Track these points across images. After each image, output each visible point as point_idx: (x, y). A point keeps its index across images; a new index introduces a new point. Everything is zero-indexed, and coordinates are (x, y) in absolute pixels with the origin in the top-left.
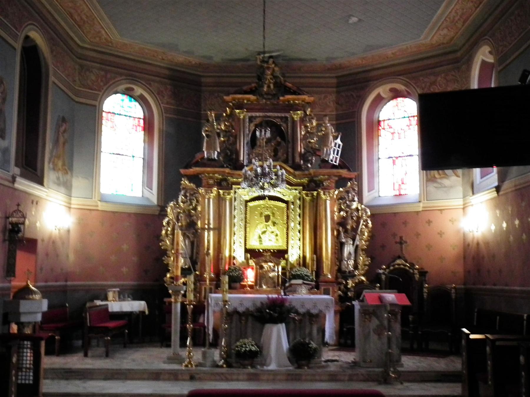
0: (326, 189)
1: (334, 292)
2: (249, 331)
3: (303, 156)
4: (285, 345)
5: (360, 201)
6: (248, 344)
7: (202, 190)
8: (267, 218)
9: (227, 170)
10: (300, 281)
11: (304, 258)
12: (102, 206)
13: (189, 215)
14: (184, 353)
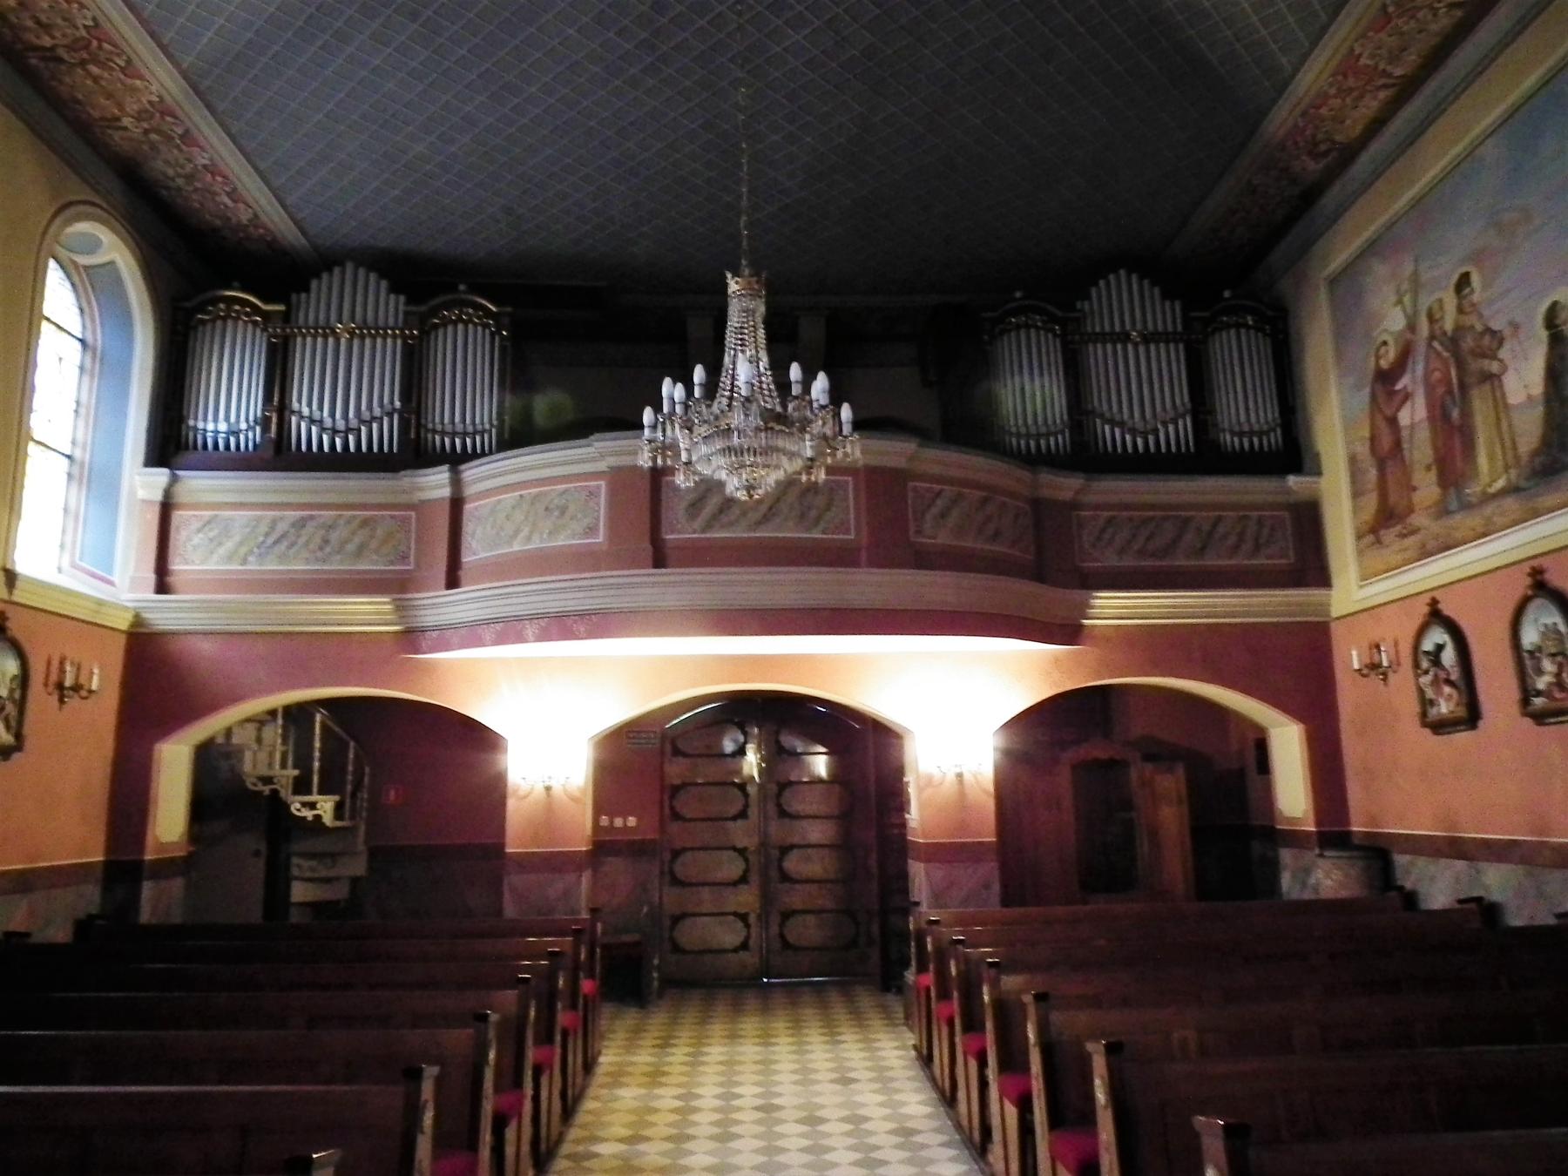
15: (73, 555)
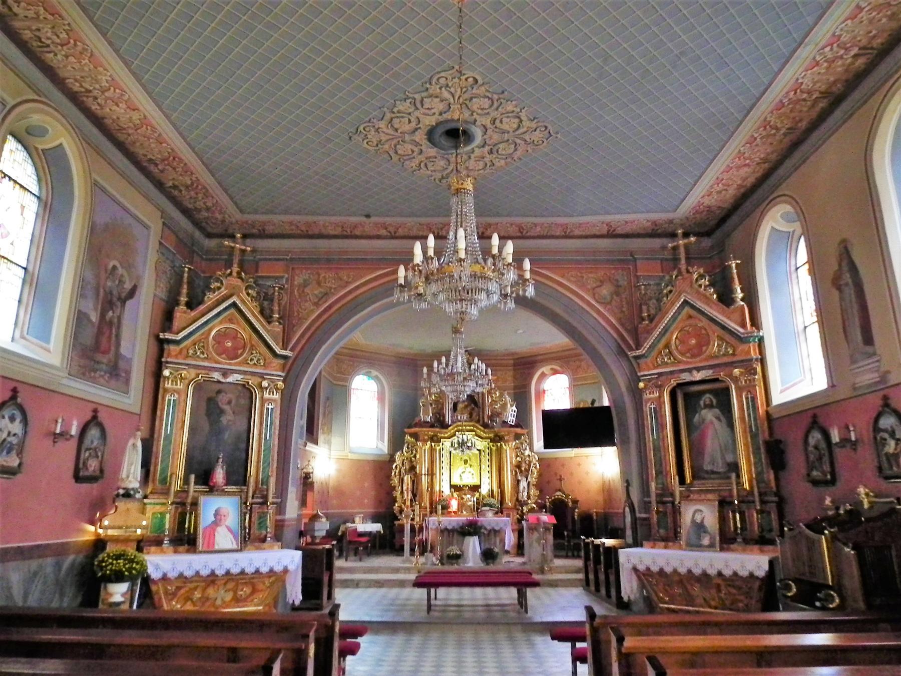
0: (506, 442)
1: (513, 516)
2: (455, 541)
3: (490, 418)
4: (478, 550)
5: (531, 450)
6: (455, 550)
7: (420, 444)
8: (466, 462)
9: (438, 430)
10: (488, 508)
11: (492, 491)
12: (351, 456)
13: (411, 461)
14: (414, 559)
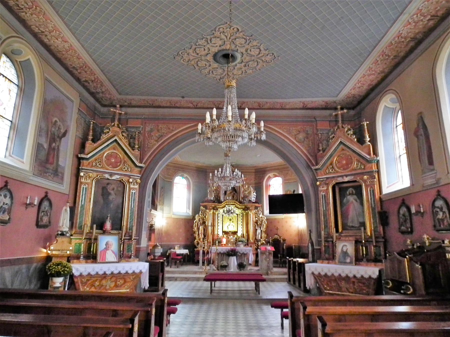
0: (251, 210)
3: (242, 198)
5: (263, 214)
6: (224, 263)
9: (217, 204)
10: (241, 243)
11: (243, 235)
12: (173, 216)
13: (203, 219)
15: (10, 153)
